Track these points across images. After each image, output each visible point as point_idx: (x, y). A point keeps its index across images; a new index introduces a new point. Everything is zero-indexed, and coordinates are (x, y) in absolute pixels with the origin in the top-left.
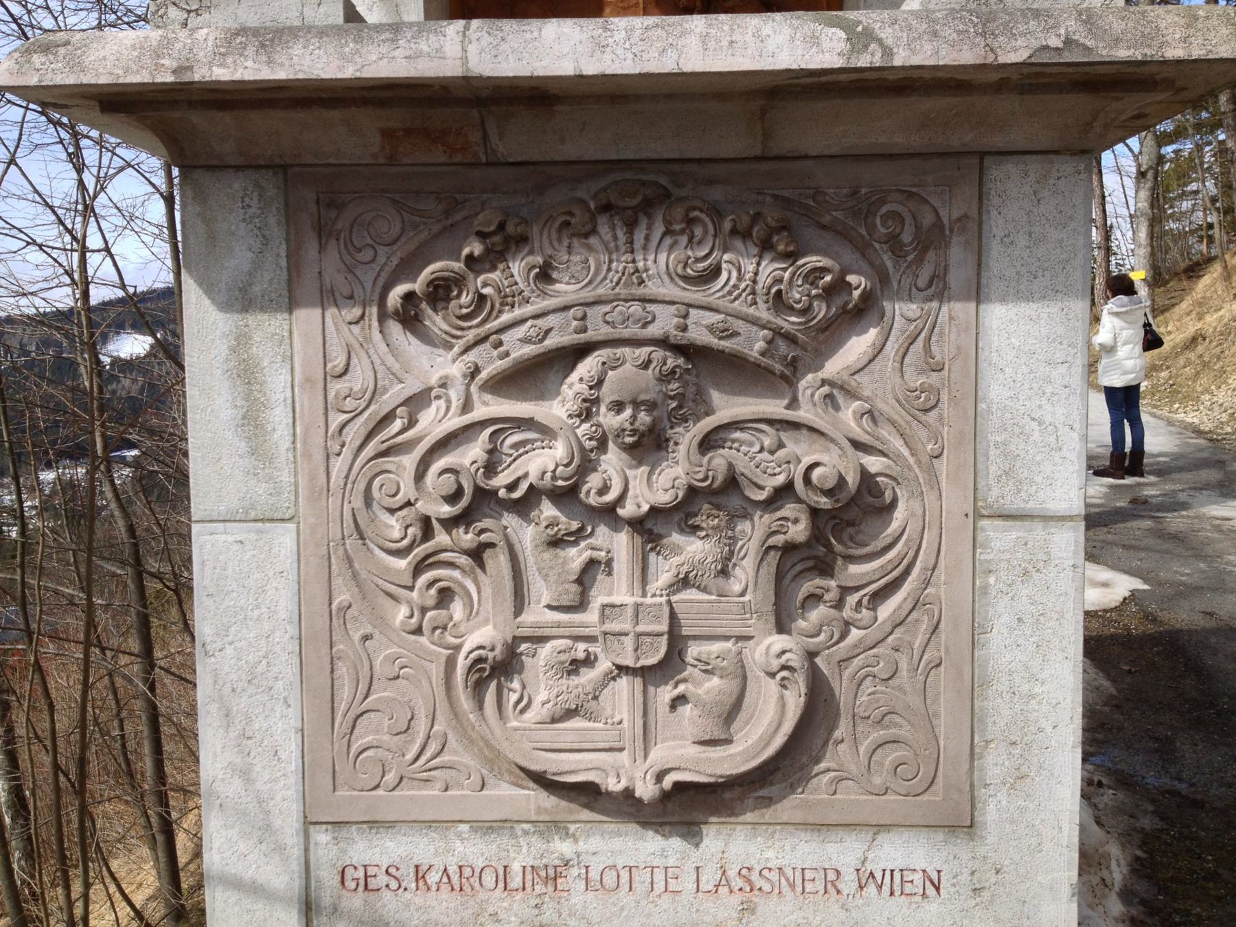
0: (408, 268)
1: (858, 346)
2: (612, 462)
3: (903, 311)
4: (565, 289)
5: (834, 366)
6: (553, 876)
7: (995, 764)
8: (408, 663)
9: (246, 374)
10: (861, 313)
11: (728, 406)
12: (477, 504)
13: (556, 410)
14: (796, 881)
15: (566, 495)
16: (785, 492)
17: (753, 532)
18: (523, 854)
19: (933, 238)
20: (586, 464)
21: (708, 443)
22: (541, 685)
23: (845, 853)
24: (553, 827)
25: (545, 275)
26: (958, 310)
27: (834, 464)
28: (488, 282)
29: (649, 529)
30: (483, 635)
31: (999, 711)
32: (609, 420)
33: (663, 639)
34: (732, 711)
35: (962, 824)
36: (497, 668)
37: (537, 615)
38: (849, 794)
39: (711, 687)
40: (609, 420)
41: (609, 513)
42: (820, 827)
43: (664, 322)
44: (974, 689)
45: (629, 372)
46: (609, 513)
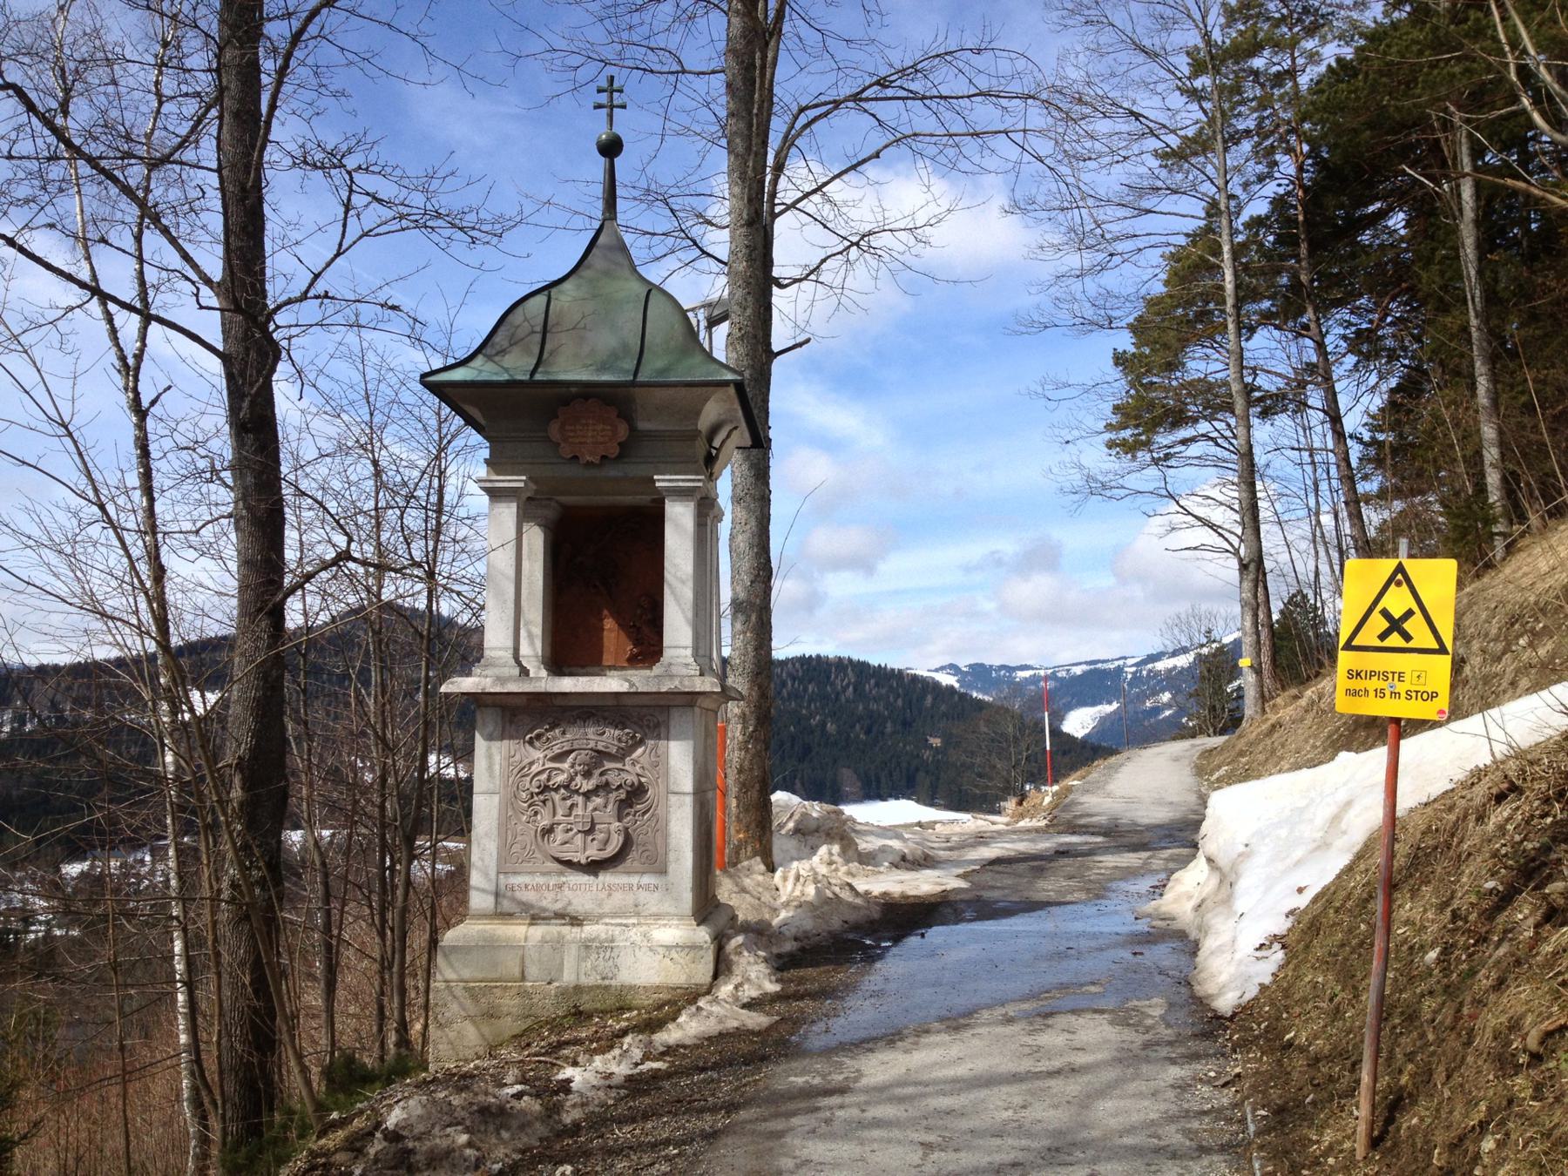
0: (531, 731)
1: (640, 751)
2: (579, 779)
3: (651, 743)
4: (568, 736)
5: (634, 756)
6: (560, 887)
7: (672, 856)
8: (526, 830)
9: (490, 757)
10: (641, 742)
11: (608, 765)
12: (545, 789)
13: (566, 766)
14: (622, 888)
15: (567, 787)
16: (620, 787)
17: (613, 796)
18: (553, 881)
19: (657, 725)
20: (572, 779)
21: (602, 774)
22: (559, 835)
23: (634, 880)
24: (561, 873)
25: (564, 733)
26: (662, 743)
27: (631, 778)
28: (550, 735)
29: (587, 795)
30: (544, 821)
31: (673, 842)
32: (578, 768)
33: (587, 823)
34: (606, 842)
35: (663, 871)
36: (548, 831)
37: (559, 817)
38: (636, 864)
39: (601, 836)
40: (578, 768)
41: (577, 792)
42: (628, 873)
43: (592, 744)
44: (666, 836)
45: (583, 756)
46: (577, 792)
